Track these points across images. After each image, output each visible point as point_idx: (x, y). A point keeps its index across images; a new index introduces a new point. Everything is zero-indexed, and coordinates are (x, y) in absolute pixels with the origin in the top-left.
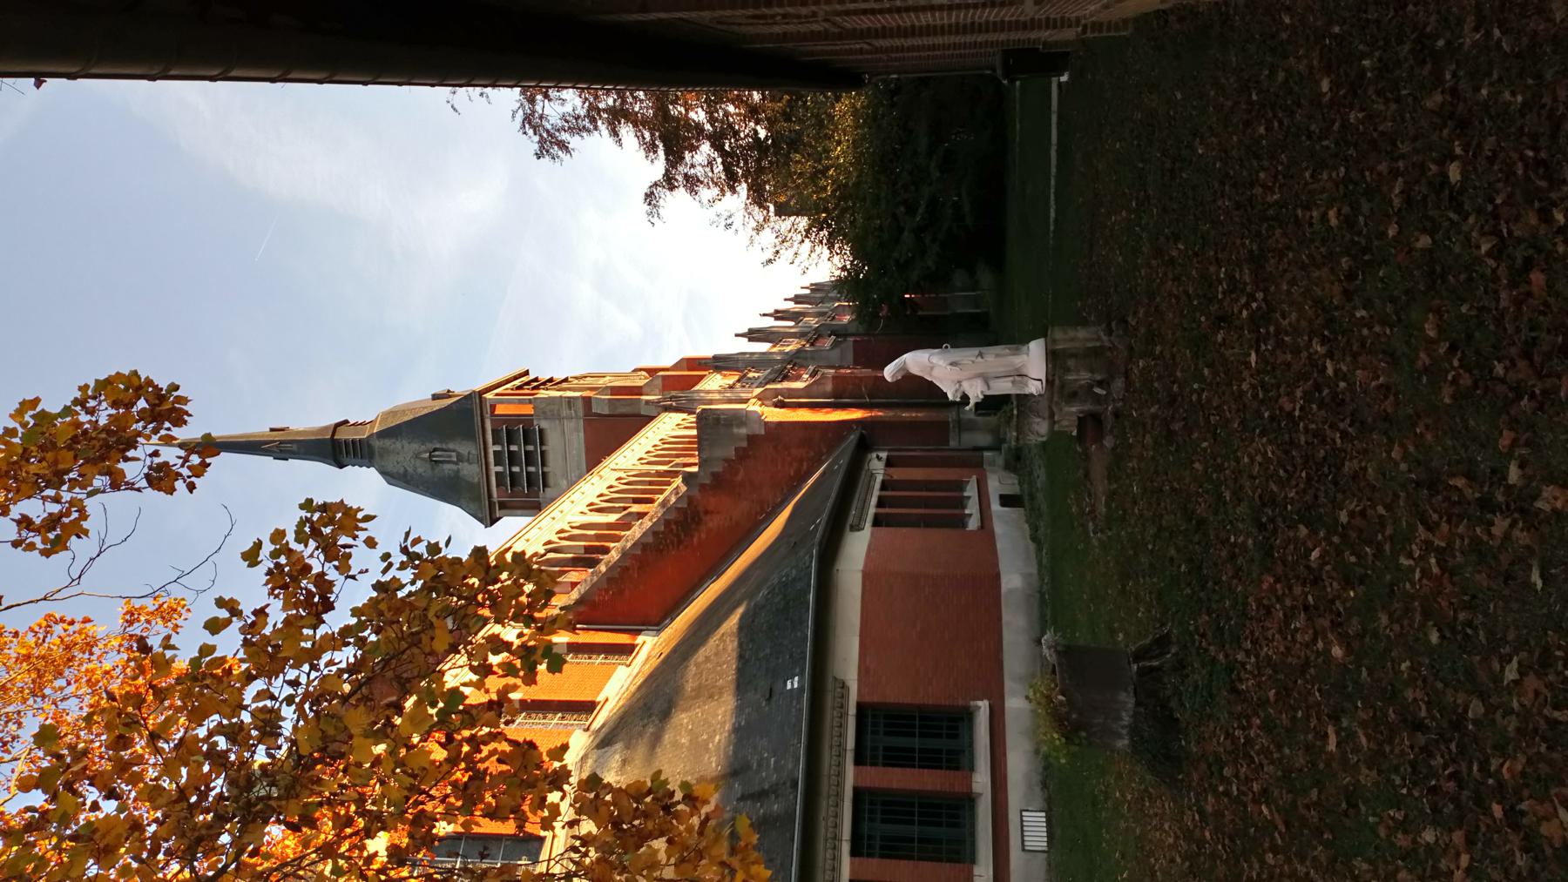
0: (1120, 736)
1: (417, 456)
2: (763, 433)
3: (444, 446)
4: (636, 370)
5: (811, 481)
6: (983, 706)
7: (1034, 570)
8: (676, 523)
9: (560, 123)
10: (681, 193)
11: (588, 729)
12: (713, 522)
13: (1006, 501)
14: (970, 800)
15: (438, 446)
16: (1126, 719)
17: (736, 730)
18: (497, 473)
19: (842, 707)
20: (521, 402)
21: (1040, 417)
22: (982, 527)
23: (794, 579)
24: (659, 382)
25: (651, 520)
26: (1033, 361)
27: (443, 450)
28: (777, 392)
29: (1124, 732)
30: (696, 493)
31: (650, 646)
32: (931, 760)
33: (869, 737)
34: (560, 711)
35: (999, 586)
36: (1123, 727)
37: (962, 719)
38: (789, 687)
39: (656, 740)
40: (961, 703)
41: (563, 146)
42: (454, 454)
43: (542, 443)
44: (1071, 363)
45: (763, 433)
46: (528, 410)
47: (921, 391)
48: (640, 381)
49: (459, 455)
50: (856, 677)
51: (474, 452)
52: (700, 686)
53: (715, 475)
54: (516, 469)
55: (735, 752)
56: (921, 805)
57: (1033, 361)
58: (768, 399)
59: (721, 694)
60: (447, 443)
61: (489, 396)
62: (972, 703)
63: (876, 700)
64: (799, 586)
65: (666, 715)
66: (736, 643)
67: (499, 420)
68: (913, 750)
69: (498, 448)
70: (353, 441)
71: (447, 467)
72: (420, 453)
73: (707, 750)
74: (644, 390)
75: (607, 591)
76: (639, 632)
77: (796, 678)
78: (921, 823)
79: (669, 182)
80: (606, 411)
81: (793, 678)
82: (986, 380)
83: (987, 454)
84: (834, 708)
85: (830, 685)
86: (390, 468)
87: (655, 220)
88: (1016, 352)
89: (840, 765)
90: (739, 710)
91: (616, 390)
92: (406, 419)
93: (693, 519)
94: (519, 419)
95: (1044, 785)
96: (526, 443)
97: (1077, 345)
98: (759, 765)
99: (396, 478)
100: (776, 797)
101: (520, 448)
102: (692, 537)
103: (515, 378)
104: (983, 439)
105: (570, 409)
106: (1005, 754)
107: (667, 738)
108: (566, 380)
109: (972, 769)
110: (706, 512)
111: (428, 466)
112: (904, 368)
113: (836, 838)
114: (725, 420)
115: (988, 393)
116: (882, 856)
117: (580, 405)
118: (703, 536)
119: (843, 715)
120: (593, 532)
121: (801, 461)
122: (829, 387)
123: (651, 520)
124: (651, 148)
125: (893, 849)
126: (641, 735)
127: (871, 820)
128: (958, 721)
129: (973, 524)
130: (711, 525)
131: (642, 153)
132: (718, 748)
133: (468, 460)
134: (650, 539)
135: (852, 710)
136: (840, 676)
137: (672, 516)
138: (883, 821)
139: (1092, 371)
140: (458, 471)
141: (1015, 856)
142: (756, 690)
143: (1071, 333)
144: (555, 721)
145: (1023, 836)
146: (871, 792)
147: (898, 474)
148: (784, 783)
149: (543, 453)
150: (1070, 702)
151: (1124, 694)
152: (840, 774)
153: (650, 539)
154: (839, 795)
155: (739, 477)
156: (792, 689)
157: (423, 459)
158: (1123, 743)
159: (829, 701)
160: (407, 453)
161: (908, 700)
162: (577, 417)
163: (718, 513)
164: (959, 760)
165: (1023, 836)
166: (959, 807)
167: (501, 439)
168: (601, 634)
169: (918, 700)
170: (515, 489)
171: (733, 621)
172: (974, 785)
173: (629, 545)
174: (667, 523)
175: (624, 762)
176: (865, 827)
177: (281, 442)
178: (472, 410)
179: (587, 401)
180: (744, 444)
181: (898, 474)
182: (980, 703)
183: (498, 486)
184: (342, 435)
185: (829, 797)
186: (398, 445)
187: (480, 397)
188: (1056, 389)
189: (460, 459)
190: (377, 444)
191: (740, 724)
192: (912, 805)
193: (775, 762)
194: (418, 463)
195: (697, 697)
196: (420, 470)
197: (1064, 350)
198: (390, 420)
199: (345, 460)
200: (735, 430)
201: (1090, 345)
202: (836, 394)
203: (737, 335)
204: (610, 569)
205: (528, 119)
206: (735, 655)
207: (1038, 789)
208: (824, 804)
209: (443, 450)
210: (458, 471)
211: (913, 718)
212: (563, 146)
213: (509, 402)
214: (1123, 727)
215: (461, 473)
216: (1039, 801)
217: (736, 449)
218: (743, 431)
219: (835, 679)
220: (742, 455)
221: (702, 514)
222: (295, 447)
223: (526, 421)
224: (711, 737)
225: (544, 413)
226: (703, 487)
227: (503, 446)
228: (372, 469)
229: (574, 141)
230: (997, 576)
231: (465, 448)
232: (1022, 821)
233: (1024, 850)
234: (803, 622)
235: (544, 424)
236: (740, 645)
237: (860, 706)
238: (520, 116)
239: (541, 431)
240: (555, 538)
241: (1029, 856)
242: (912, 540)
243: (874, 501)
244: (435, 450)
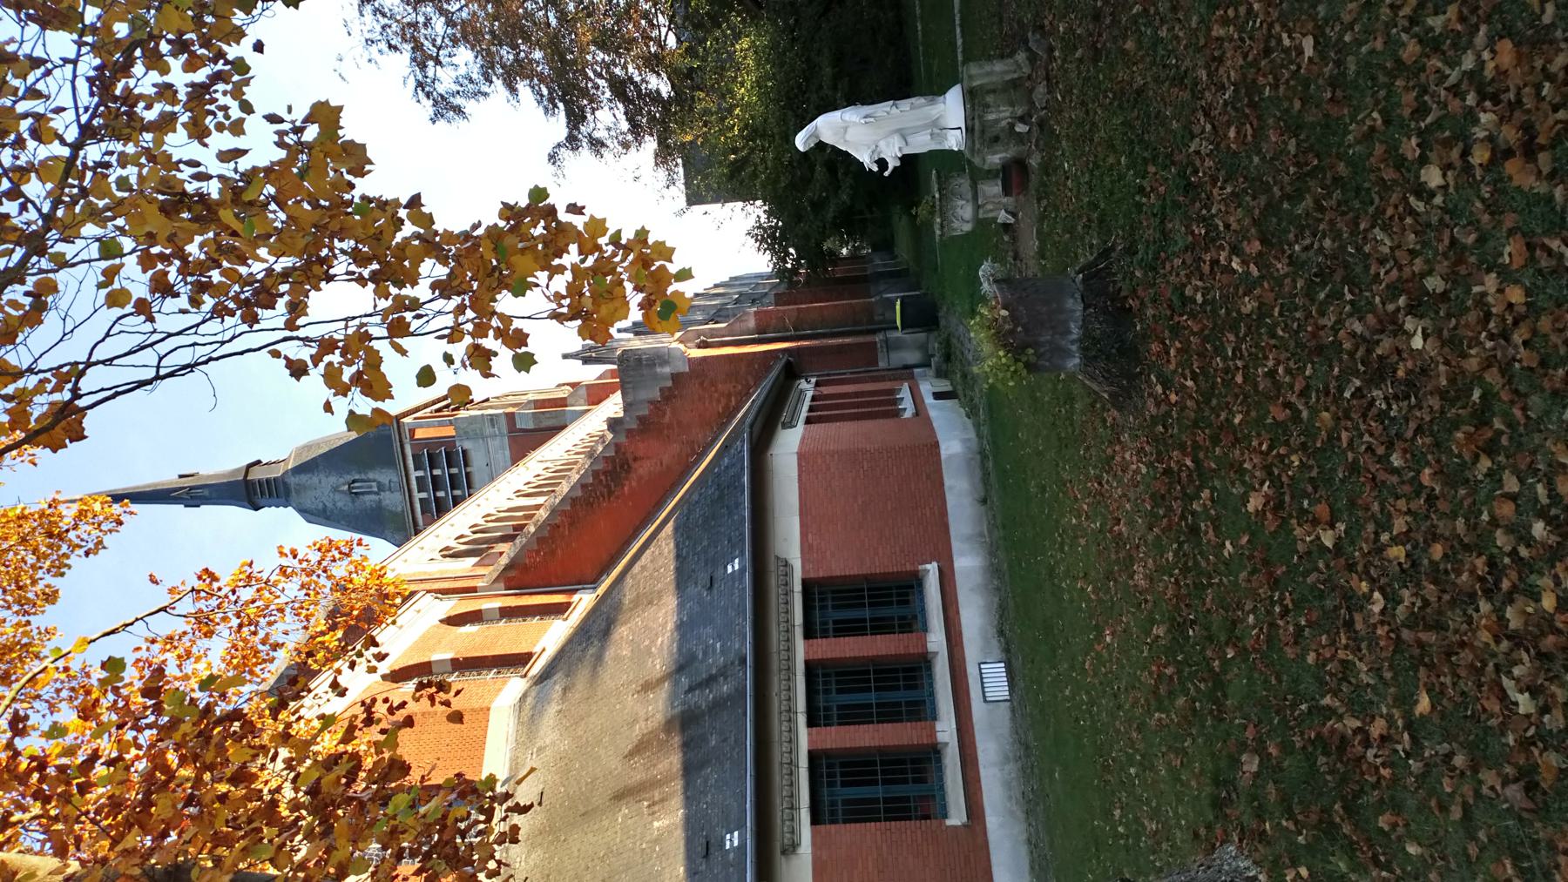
0: (1070, 355)
1: (335, 489)
2: (687, 370)
3: (363, 477)
4: (559, 386)
5: (740, 415)
6: (932, 568)
7: (972, 435)
8: (605, 473)
9: (456, 88)
10: (585, 151)
11: (525, 676)
12: (643, 469)
13: (938, 396)
14: (934, 752)
15: (357, 477)
16: (1075, 331)
17: (680, 626)
18: (421, 500)
19: (786, 584)
20: (441, 424)
21: (962, 199)
22: (917, 414)
23: (727, 467)
24: (583, 392)
25: (578, 473)
26: (951, 108)
27: (362, 481)
28: (699, 334)
29: (1074, 348)
30: (623, 439)
31: (584, 601)
32: (889, 714)
33: (825, 790)
34: (495, 667)
35: (938, 454)
36: (1073, 342)
37: (912, 587)
38: (730, 569)
39: (599, 658)
40: (909, 567)
41: (458, 110)
42: (374, 484)
43: (466, 465)
44: (990, 99)
45: (687, 370)
46: (449, 431)
47: (834, 159)
48: (564, 393)
49: (380, 486)
50: (798, 555)
51: (395, 479)
52: (638, 596)
53: (641, 419)
54: (441, 494)
55: (680, 649)
56: (875, 672)
57: (951, 108)
58: (689, 341)
59: (660, 598)
60: (366, 473)
61: (407, 420)
62: (920, 567)
63: (821, 574)
64: (732, 472)
65: (606, 633)
66: (672, 545)
67: (419, 445)
68: (864, 620)
69: (421, 473)
70: (268, 481)
71: (367, 498)
72: (338, 487)
73: (650, 653)
74: (569, 402)
75: (538, 552)
76: (575, 591)
77: (737, 561)
78: (885, 782)
79: (572, 141)
80: (531, 426)
81: (733, 561)
82: (904, 135)
83: (916, 371)
84: (780, 671)
85: (772, 566)
86: (308, 504)
87: (561, 180)
88: (932, 102)
89: (790, 640)
90: (681, 606)
91: (539, 404)
92: (321, 451)
93: (622, 467)
94: (439, 441)
95: (1001, 633)
96: (449, 466)
97: (994, 79)
98: (705, 653)
99: (314, 515)
100: (726, 679)
101: (443, 473)
102: (623, 486)
103: (434, 403)
104: (912, 357)
105: (493, 426)
106: (958, 612)
107: (610, 654)
108: (487, 400)
109: (925, 630)
110: (635, 459)
111: (348, 499)
112: (815, 134)
113: (791, 711)
114: (647, 360)
115: (908, 151)
116: (840, 724)
117: (503, 421)
118: (634, 484)
119: (788, 593)
120: (521, 514)
121: (729, 395)
122: (752, 323)
123: (578, 473)
124: (550, 109)
125: (860, 813)
126: (580, 659)
127: (831, 785)
128: (910, 586)
129: (908, 414)
130: (641, 471)
131: (541, 110)
132: (661, 649)
133: (390, 489)
134: (579, 493)
135: (798, 587)
136: (783, 556)
137: (600, 466)
138: (844, 784)
139: (1012, 104)
140: (380, 501)
141: (977, 707)
142: (696, 584)
143: (988, 68)
144: (491, 675)
145: (983, 688)
146: (827, 753)
147: (826, 390)
148: (732, 663)
149: (468, 474)
150: (1014, 317)
151: (1071, 301)
152: (790, 649)
153: (579, 493)
154: (790, 670)
155: (667, 419)
156: (734, 572)
157: (343, 492)
158: (1074, 362)
159: (773, 581)
160: (325, 487)
161: (855, 571)
162: (501, 435)
163: (648, 458)
164: (913, 623)
165: (983, 688)
166: (916, 669)
167: (424, 463)
168: (534, 597)
169: (864, 571)
171: (670, 527)
172: (929, 645)
173: (557, 501)
174: (596, 474)
175: (565, 690)
176: (821, 701)
177: (191, 488)
178: (390, 436)
179: (510, 417)
180: (669, 384)
181: (826, 390)
182: (928, 566)
184: (256, 475)
185: (780, 671)
186: (315, 479)
187: (398, 422)
188: (977, 134)
189: (381, 488)
190: (292, 481)
191: (681, 620)
192: (868, 672)
193: (721, 646)
194: (337, 497)
195: (636, 606)
196: (339, 504)
197: (981, 86)
198: (304, 454)
199: (261, 502)
200: (659, 370)
201: (1008, 78)
202: (761, 329)
204: (539, 529)
205: (420, 85)
206: (672, 556)
207: (995, 642)
208: (776, 679)
209: (362, 481)
210: (380, 501)
211: (874, 763)
212: (458, 110)
213: (429, 426)
214: (1073, 342)
215: (384, 503)
216: (997, 652)
217: (661, 390)
218: (667, 370)
219: (777, 558)
220: (668, 396)
221: (630, 461)
222: (206, 492)
223: (448, 443)
224: (653, 642)
225: (466, 433)
226: (629, 432)
227: (425, 470)
228: (290, 508)
229: (469, 106)
230: (937, 445)
231: (385, 476)
232: (981, 674)
233: (985, 701)
234: (738, 505)
235: (467, 445)
236: (677, 545)
237: (805, 582)
238: (412, 83)
239: (464, 452)
240: (481, 522)
241: (991, 706)
242: (843, 433)
243: (805, 408)
244: (354, 482)
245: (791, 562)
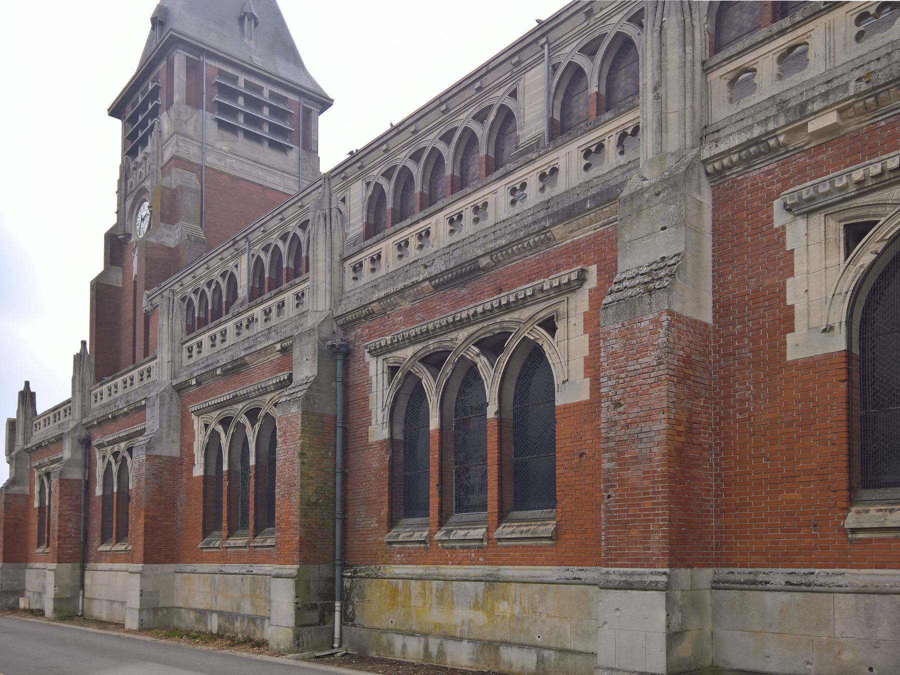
235: (293, 155)
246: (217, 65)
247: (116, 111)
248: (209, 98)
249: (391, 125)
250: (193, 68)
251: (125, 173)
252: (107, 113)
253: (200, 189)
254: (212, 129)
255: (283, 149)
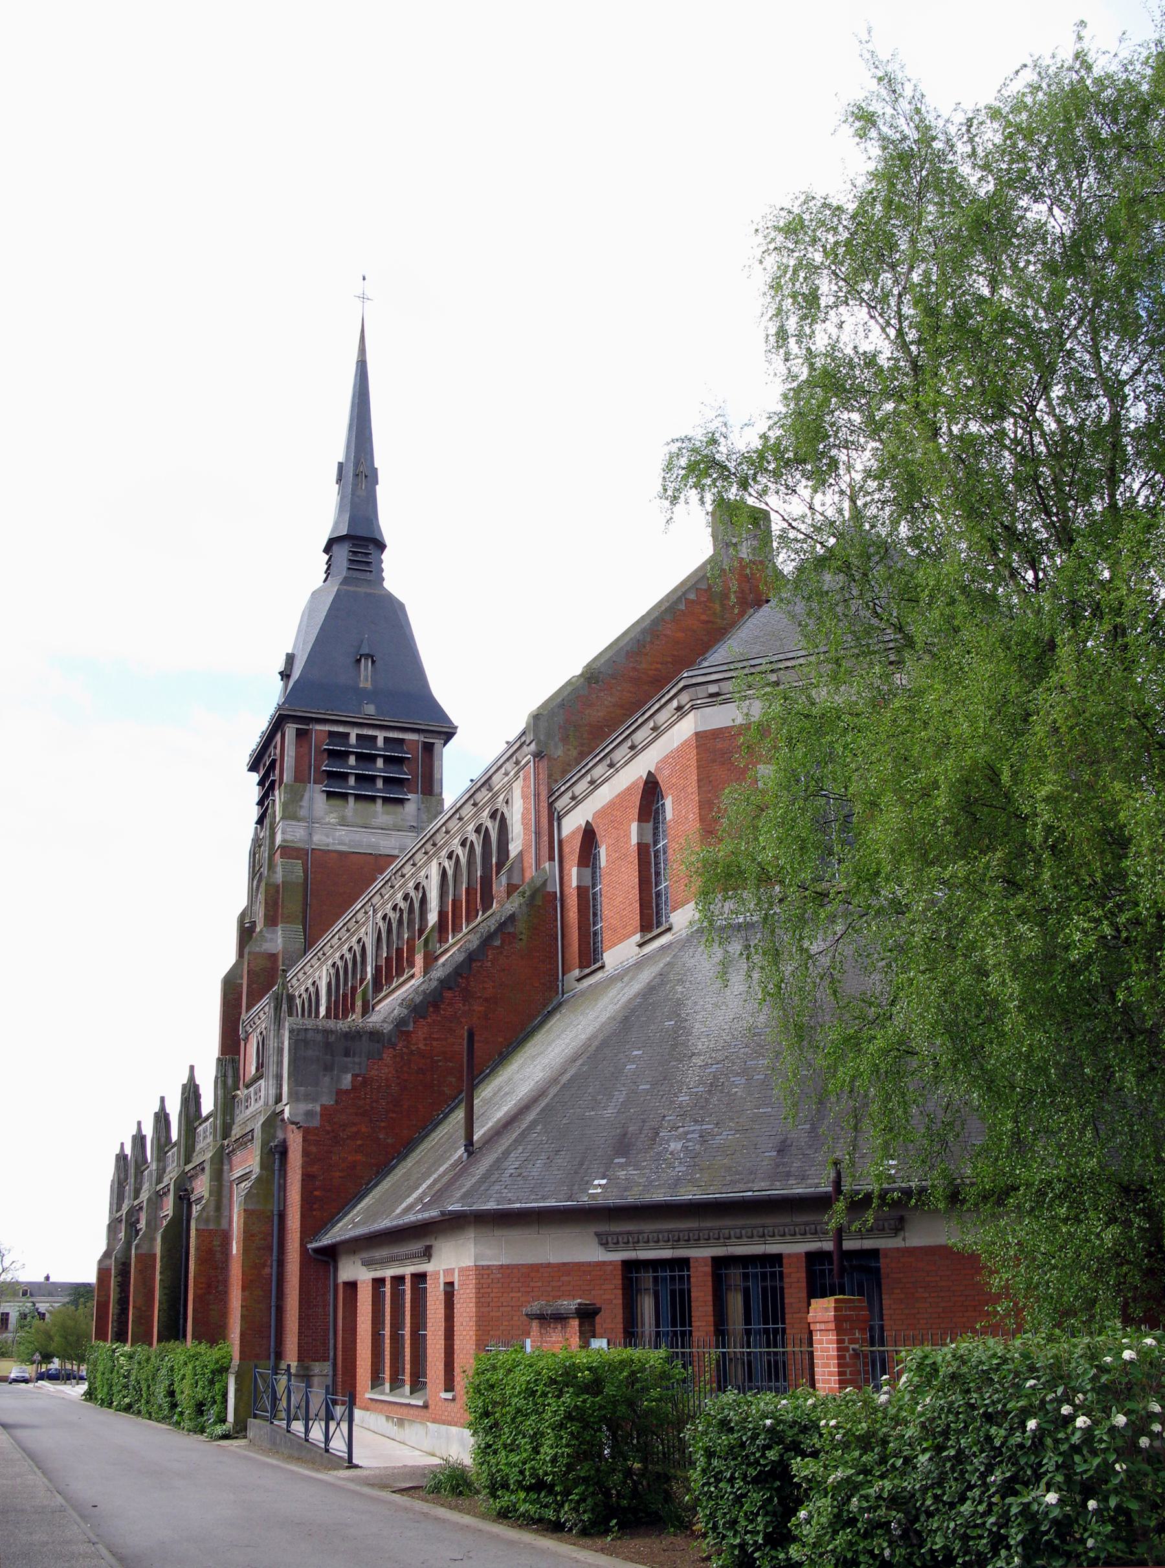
170: (325, 755)
183: (331, 733)
203: (192, 1068)
235: (410, 808)
245: (433, 1260)
246: (327, 728)
247: (253, 768)
248: (317, 768)
249: (507, 743)
250: (301, 735)
251: (257, 843)
252: (246, 768)
253: (301, 881)
254: (320, 801)
255: (401, 802)
